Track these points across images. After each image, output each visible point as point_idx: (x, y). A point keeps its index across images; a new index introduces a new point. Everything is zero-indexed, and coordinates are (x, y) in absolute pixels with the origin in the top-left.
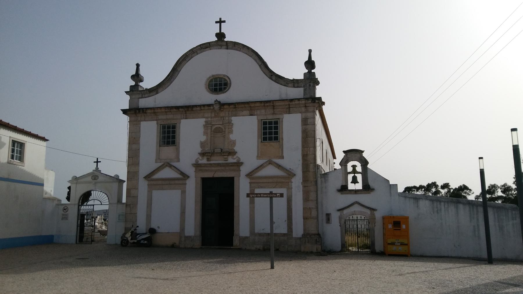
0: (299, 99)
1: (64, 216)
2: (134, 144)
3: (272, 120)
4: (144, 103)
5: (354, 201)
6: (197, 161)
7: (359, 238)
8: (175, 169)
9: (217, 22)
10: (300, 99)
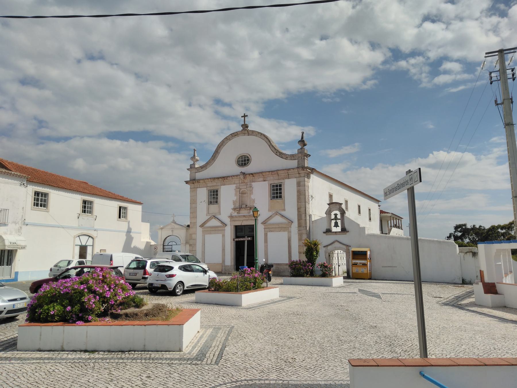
0: (293, 169)
1: (155, 253)
2: (193, 204)
3: (277, 184)
4: (199, 175)
5: (335, 240)
6: (231, 215)
7: (339, 267)
8: (218, 220)
9: (242, 117)
10: (294, 168)
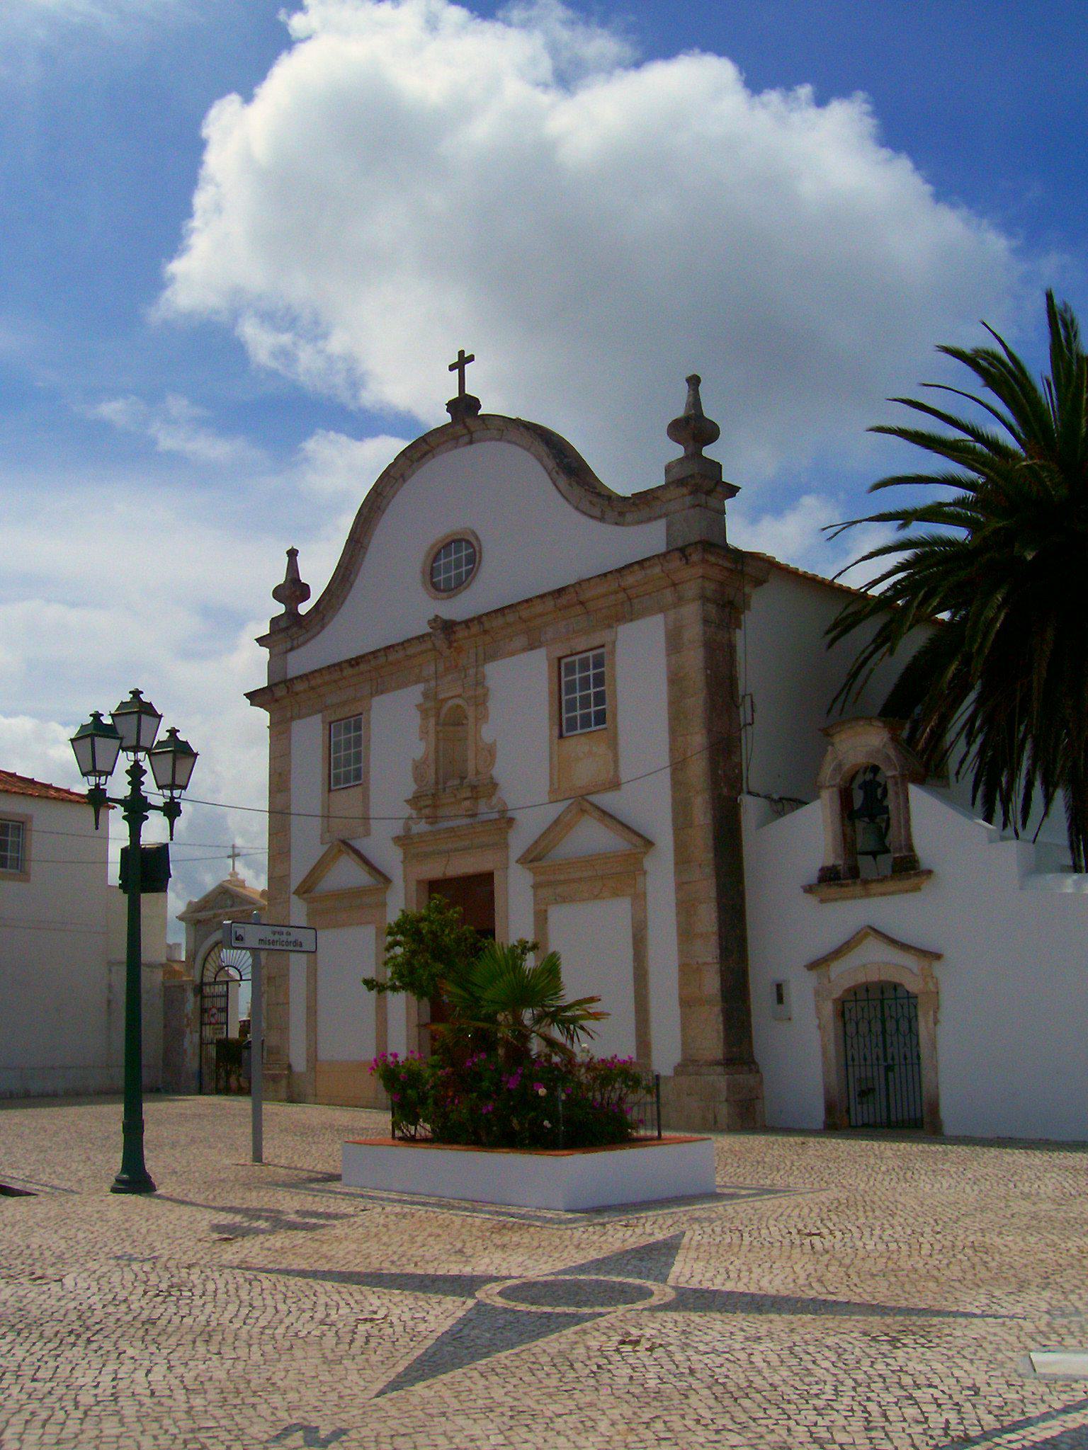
7: (890, 1074)
